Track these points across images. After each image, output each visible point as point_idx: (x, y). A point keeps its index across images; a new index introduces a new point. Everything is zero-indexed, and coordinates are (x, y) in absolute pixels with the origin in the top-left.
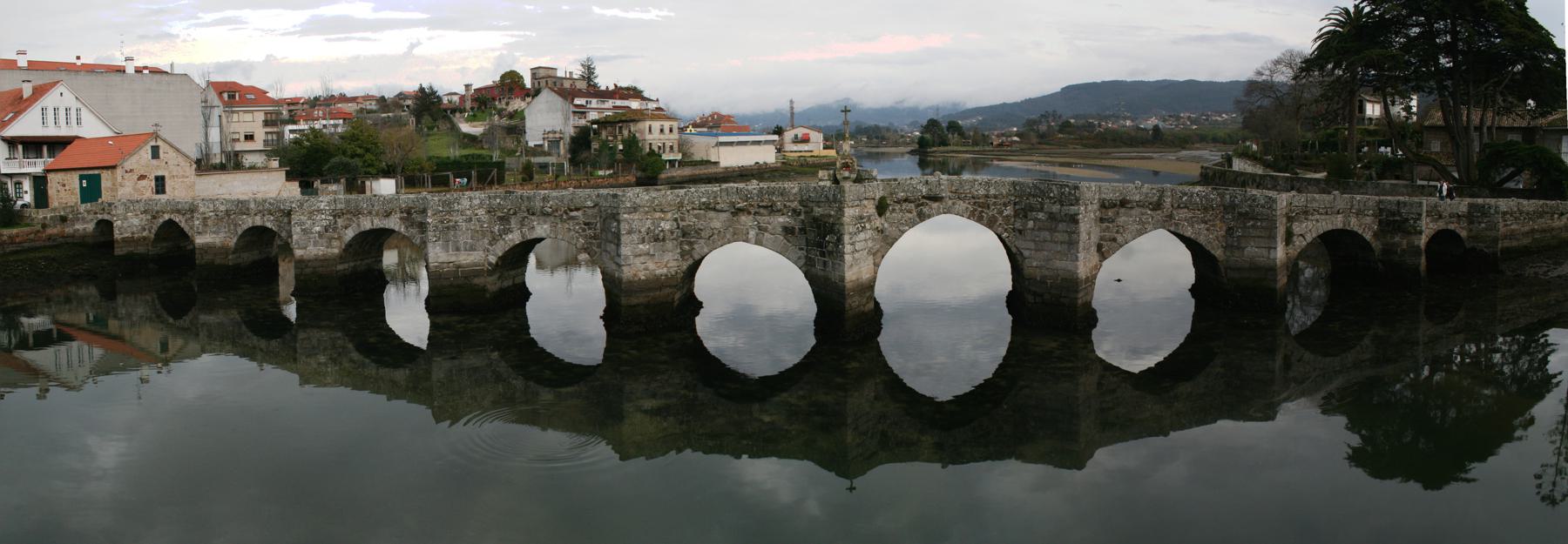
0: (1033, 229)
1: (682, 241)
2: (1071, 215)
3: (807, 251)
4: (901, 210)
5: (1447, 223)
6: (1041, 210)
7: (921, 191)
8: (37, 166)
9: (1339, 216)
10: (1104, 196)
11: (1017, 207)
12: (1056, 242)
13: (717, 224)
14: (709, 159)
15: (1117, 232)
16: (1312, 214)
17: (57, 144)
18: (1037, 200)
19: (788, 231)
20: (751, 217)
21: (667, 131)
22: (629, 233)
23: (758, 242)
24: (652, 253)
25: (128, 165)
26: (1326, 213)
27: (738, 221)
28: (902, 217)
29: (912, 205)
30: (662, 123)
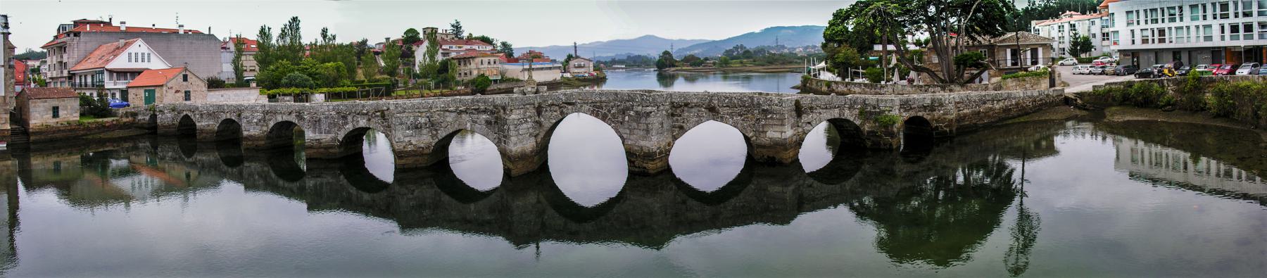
5: (916, 112)
8: (122, 85)
13: (449, 119)
15: (683, 122)
16: (816, 109)
17: (135, 73)
19: (488, 123)
20: (468, 115)
21: (492, 63)
25: (169, 85)
26: (826, 108)
27: (461, 117)
29: (557, 107)
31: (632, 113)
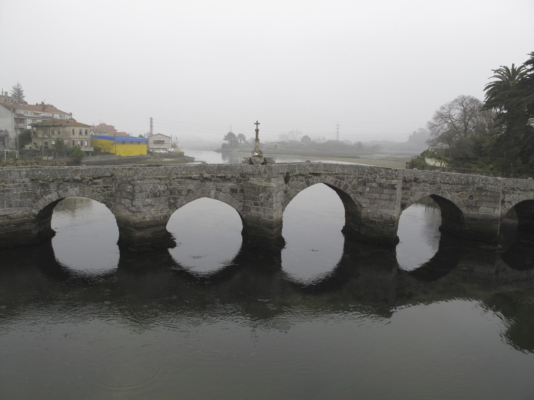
0: (369, 192)
1: (170, 197)
2: (392, 185)
3: (244, 202)
4: (297, 180)
6: (375, 181)
7: (309, 170)
9: (531, 192)
10: (405, 175)
11: (360, 180)
12: (382, 200)
14: (109, 152)
18: (372, 176)
19: (233, 191)
20: (212, 183)
21: (84, 133)
22: (141, 192)
23: (216, 198)
24: (153, 204)
26: (525, 190)
28: (298, 184)
29: (304, 178)
30: (80, 128)
31: (374, 185)
